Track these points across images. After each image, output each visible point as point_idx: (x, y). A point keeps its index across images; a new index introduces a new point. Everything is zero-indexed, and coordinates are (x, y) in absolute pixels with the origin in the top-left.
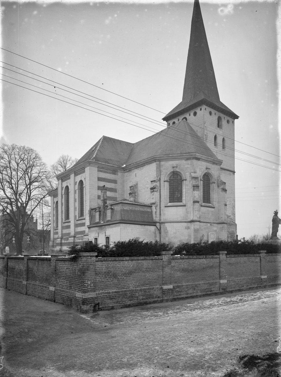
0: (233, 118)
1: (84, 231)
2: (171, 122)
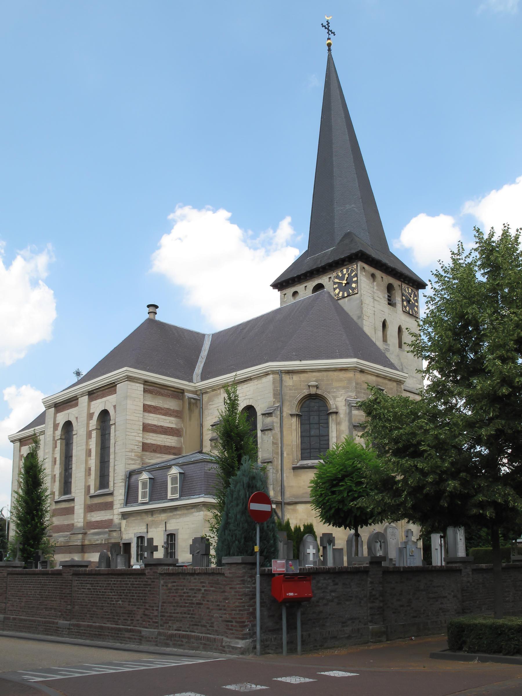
0: (415, 287)
1: (111, 521)
2: (290, 291)
